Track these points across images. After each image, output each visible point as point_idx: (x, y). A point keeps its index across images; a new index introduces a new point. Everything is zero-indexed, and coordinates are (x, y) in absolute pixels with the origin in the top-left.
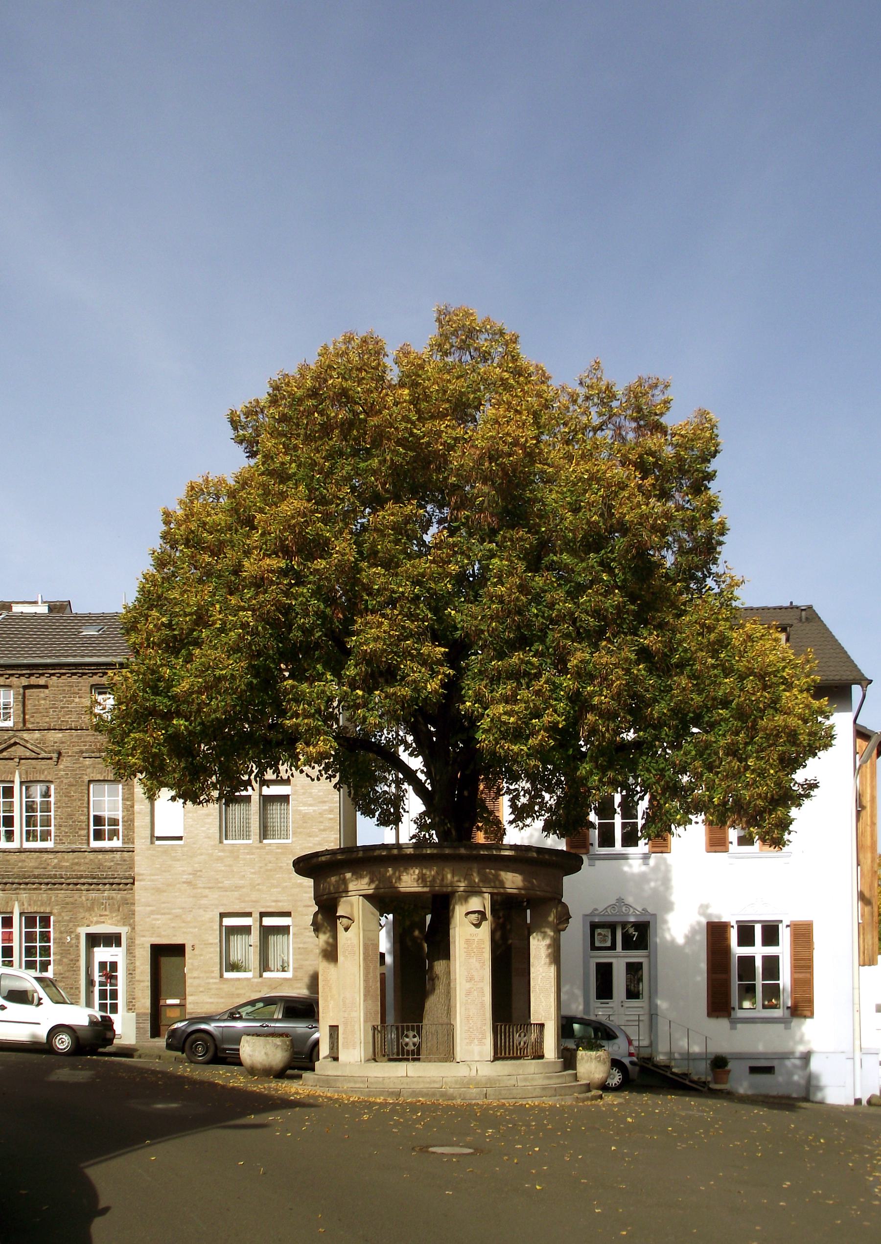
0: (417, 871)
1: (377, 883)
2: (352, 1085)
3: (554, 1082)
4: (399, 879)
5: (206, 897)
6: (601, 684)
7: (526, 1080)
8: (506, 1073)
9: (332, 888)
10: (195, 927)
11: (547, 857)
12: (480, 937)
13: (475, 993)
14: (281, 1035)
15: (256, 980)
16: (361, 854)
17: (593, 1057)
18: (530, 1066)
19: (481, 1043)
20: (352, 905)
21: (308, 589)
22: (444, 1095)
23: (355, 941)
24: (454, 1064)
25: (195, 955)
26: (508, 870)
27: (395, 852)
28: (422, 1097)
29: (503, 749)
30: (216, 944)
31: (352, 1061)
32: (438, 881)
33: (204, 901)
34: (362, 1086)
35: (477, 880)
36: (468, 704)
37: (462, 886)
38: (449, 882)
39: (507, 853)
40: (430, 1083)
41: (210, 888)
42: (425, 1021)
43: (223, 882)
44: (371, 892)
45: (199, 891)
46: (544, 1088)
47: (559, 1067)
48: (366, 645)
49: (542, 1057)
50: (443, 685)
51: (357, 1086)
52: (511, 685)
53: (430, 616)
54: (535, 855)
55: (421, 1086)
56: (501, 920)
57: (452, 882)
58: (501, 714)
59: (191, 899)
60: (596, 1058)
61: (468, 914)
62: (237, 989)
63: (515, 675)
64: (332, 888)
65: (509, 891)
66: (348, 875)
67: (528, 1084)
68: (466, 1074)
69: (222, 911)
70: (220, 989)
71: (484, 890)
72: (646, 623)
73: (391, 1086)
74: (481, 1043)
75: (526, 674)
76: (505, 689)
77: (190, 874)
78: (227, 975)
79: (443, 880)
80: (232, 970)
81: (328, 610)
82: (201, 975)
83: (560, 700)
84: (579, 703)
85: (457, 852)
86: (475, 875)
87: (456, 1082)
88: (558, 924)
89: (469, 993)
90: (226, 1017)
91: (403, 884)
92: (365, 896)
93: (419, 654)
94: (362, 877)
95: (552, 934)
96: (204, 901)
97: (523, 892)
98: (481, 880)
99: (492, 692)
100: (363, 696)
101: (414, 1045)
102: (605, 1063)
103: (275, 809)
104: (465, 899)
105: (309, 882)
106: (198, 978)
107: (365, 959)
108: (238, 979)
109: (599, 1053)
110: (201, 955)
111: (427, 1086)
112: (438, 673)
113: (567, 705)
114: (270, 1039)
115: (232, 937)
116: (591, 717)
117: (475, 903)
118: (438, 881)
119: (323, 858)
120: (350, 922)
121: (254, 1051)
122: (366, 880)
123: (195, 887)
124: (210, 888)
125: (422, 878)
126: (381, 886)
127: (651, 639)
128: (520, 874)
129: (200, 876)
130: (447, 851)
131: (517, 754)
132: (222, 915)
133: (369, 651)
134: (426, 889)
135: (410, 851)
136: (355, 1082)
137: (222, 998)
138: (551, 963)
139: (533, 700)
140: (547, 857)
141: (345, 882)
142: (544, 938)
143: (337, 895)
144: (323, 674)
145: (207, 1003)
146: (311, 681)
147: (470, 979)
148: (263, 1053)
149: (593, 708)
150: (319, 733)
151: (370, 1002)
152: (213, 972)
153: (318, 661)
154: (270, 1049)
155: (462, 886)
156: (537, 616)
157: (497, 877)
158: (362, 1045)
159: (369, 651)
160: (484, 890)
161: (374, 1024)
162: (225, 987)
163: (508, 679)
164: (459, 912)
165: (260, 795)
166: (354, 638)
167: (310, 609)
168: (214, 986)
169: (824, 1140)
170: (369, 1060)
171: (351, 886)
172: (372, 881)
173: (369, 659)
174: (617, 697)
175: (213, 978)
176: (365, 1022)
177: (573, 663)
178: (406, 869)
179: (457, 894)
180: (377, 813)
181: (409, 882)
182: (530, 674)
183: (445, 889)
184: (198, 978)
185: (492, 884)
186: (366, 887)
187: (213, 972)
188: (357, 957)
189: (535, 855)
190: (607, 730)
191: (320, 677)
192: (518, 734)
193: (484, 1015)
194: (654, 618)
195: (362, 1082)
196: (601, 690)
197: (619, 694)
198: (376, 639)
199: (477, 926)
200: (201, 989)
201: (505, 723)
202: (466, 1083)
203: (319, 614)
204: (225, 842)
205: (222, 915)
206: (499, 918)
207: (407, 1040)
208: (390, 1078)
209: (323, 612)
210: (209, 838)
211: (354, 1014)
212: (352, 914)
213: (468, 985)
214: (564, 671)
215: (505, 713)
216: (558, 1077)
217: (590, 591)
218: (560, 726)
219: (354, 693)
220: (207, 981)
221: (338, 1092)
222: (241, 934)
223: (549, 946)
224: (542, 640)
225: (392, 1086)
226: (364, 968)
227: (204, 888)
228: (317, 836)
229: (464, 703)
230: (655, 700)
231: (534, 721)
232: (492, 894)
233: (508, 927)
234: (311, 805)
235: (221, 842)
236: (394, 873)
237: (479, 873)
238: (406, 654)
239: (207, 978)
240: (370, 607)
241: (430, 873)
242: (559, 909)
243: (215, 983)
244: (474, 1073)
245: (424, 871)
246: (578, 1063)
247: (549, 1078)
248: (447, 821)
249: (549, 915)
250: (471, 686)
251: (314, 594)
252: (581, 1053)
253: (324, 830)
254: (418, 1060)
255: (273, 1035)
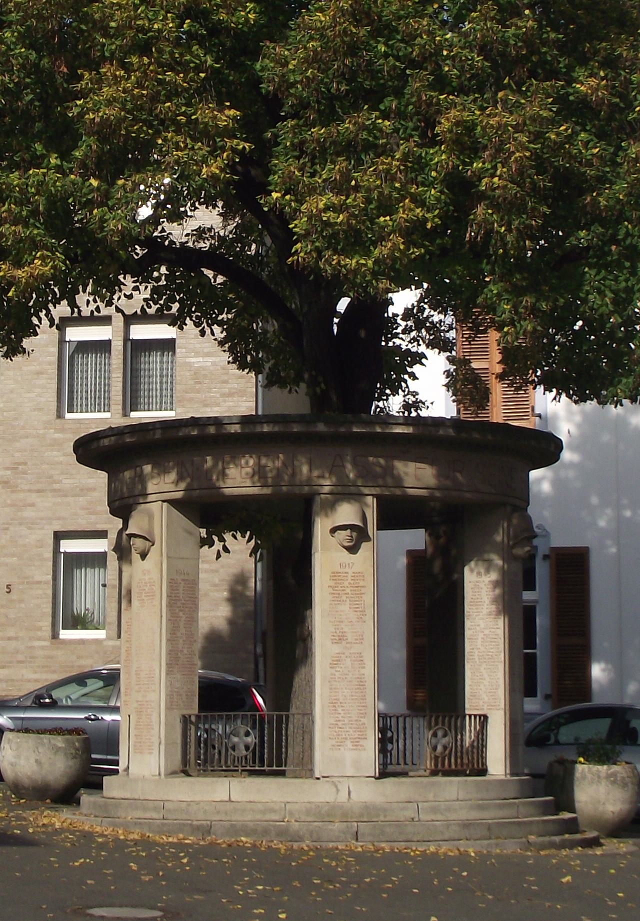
0: (251, 462)
1: (188, 480)
2: (139, 814)
3: (490, 816)
4: (223, 475)
5: (33, 505)
6: (494, 157)
7: (434, 810)
8: (403, 797)
9: (125, 489)
10: (13, 555)
11: (476, 435)
12: (356, 569)
13: (348, 662)
14: (70, 732)
15: (111, 643)
16: (158, 435)
17: (603, 775)
18: (453, 788)
19: (357, 744)
20: (151, 517)
21: (13, 32)
22: (283, 833)
23: (155, 576)
24: (311, 781)
25: (12, 601)
26: (407, 457)
27: (212, 430)
28: (247, 836)
29: (330, 265)
30: (46, 583)
31: (147, 774)
32: (286, 478)
33: (29, 513)
34: (155, 815)
35: (351, 475)
36: (275, 195)
37: (327, 485)
38: (304, 478)
39: (399, 430)
40: (263, 812)
41: (38, 491)
42: (293, 710)
43: (60, 482)
44: (179, 495)
45: (21, 495)
46: (466, 825)
47: (512, 791)
48: (94, 111)
49: (483, 772)
50: (231, 167)
51: (148, 815)
52: (342, 164)
53: (209, 62)
54: (451, 432)
55: (249, 817)
56: (442, 540)
57: (310, 478)
58: (320, 211)
59: (7, 510)
60: (608, 776)
61: (334, 530)
62: (79, 657)
63: (352, 149)
64: (125, 489)
65: (411, 491)
66: (148, 468)
67: (440, 817)
68: (330, 798)
69: (58, 528)
70: (51, 657)
71: (366, 491)
72: (583, 61)
73: (199, 817)
74: (357, 744)
75: (369, 147)
76: (331, 171)
77: (7, 469)
78: (65, 634)
79: (293, 475)
80: (74, 627)
81: (45, 62)
82: (21, 634)
83: (431, 185)
84: (462, 190)
85: (312, 429)
86: (349, 466)
87: (308, 812)
88: (513, 547)
89: (336, 662)
90: (29, 703)
91: (229, 483)
92: (172, 502)
93: (189, 121)
94: (166, 471)
95: (500, 562)
96: (29, 513)
97: (438, 494)
98: (359, 476)
99: (313, 175)
100: (98, 189)
101: (247, 748)
102: (624, 785)
103: (154, 362)
104: (330, 506)
105: (102, 477)
106: (16, 638)
107: (169, 605)
108: (82, 642)
109: (615, 768)
110: (21, 601)
111: (259, 817)
112: (223, 149)
113: (441, 192)
114: (46, 738)
115: (77, 573)
116: (480, 210)
117: (346, 513)
118: (286, 478)
119: (106, 442)
120: (148, 544)
121: (18, 757)
122: (173, 476)
123: (14, 489)
124: (38, 491)
125: (260, 473)
126: (195, 486)
127: (587, 84)
128: (431, 463)
129: (25, 473)
130: (321, 427)
131: (355, 272)
132: (59, 536)
133: (97, 120)
134: (267, 491)
135: (235, 429)
136: (145, 809)
137: (54, 672)
138: (498, 613)
139: (377, 187)
140: (476, 435)
141: (142, 479)
142: (488, 571)
143: (131, 501)
144: (43, 157)
145: (29, 681)
146: (24, 166)
147: (340, 638)
148: (32, 761)
149: (482, 196)
150: (35, 245)
151: (179, 676)
152: (40, 629)
153: (38, 137)
154: (45, 755)
155: (327, 485)
156: (386, 55)
157: (389, 471)
158: (163, 748)
159: (97, 120)
160: (366, 491)
161: (186, 712)
162: (60, 654)
163: (338, 154)
164: (321, 527)
165: (126, 339)
166: (78, 102)
167: (14, 62)
168: (41, 653)
169: (439, 882)
170: (173, 773)
171: (151, 487)
172: (180, 478)
173: (105, 132)
174: (518, 178)
175: (40, 639)
176: (169, 708)
177: (444, 125)
178: (234, 459)
179: (318, 499)
180: (267, 366)
181: (239, 479)
182: (376, 146)
183: (297, 490)
184: (16, 638)
185: (380, 482)
186: (172, 487)
187: (40, 629)
188: (157, 603)
189: (451, 432)
190: (509, 230)
191: (37, 161)
192: (355, 240)
193: (364, 698)
194: (596, 52)
195: (156, 809)
196: (495, 168)
197: (521, 172)
198: (109, 103)
199: (353, 549)
200: (20, 657)
201: (327, 224)
202: (329, 813)
203: (33, 69)
204: (68, 416)
205: (59, 536)
206: (438, 537)
207: (236, 739)
208: (198, 803)
209: (36, 65)
210: (40, 409)
211: (153, 696)
212: (151, 532)
213: (336, 649)
214: (433, 142)
215: (327, 208)
216: (500, 807)
217: (474, 15)
218: (429, 226)
219: (87, 184)
220: (30, 644)
221: (115, 825)
222: (93, 567)
223: (496, 584)
224: (398, 93)
225: (201, 816)
226: (168, 620)
227: (30, 491)
228: (218, 405)
229: (269, 193)
230: (602, 180)
231: (382, 219)
232: (378, 497)
233: (454, 552)
234: (208, 355)
235: (60, 415)
236: (215, 465)
237: (355, 464)
238: (165, 123)
239: (30, 639)
240: (107, 54)
241: (272, 464)
242: (515, 521)
243: (43, 648)
244: (343, 797)
245: (264, 461)
246: (576, 783)
247: (480, 808)
248: (321, 379)
249: (497, 531)
250: (284, 166)
251: (22, 39)
252: (582, 769)
253: (231, 395)
254: (282, 774)
255: (57, 730)
